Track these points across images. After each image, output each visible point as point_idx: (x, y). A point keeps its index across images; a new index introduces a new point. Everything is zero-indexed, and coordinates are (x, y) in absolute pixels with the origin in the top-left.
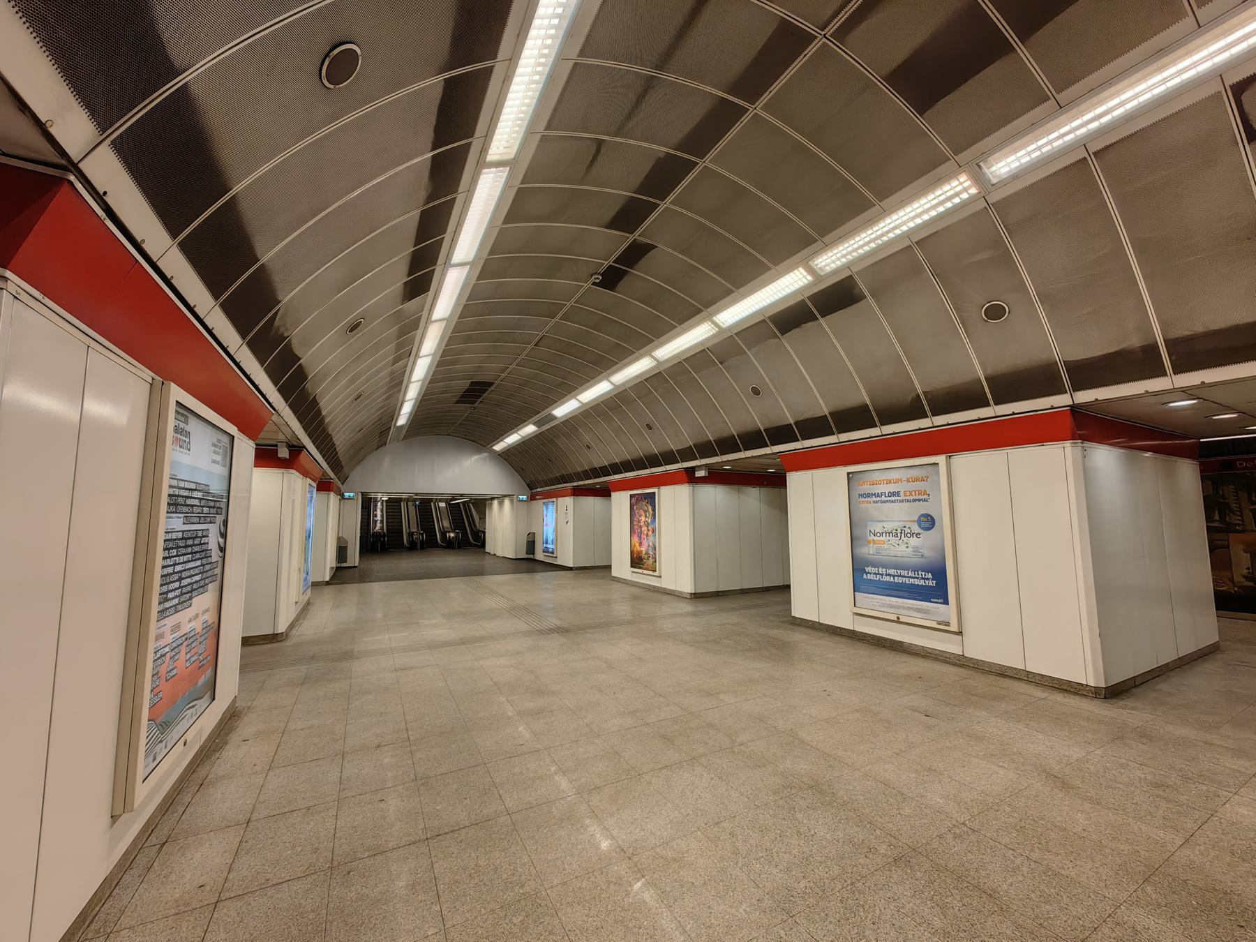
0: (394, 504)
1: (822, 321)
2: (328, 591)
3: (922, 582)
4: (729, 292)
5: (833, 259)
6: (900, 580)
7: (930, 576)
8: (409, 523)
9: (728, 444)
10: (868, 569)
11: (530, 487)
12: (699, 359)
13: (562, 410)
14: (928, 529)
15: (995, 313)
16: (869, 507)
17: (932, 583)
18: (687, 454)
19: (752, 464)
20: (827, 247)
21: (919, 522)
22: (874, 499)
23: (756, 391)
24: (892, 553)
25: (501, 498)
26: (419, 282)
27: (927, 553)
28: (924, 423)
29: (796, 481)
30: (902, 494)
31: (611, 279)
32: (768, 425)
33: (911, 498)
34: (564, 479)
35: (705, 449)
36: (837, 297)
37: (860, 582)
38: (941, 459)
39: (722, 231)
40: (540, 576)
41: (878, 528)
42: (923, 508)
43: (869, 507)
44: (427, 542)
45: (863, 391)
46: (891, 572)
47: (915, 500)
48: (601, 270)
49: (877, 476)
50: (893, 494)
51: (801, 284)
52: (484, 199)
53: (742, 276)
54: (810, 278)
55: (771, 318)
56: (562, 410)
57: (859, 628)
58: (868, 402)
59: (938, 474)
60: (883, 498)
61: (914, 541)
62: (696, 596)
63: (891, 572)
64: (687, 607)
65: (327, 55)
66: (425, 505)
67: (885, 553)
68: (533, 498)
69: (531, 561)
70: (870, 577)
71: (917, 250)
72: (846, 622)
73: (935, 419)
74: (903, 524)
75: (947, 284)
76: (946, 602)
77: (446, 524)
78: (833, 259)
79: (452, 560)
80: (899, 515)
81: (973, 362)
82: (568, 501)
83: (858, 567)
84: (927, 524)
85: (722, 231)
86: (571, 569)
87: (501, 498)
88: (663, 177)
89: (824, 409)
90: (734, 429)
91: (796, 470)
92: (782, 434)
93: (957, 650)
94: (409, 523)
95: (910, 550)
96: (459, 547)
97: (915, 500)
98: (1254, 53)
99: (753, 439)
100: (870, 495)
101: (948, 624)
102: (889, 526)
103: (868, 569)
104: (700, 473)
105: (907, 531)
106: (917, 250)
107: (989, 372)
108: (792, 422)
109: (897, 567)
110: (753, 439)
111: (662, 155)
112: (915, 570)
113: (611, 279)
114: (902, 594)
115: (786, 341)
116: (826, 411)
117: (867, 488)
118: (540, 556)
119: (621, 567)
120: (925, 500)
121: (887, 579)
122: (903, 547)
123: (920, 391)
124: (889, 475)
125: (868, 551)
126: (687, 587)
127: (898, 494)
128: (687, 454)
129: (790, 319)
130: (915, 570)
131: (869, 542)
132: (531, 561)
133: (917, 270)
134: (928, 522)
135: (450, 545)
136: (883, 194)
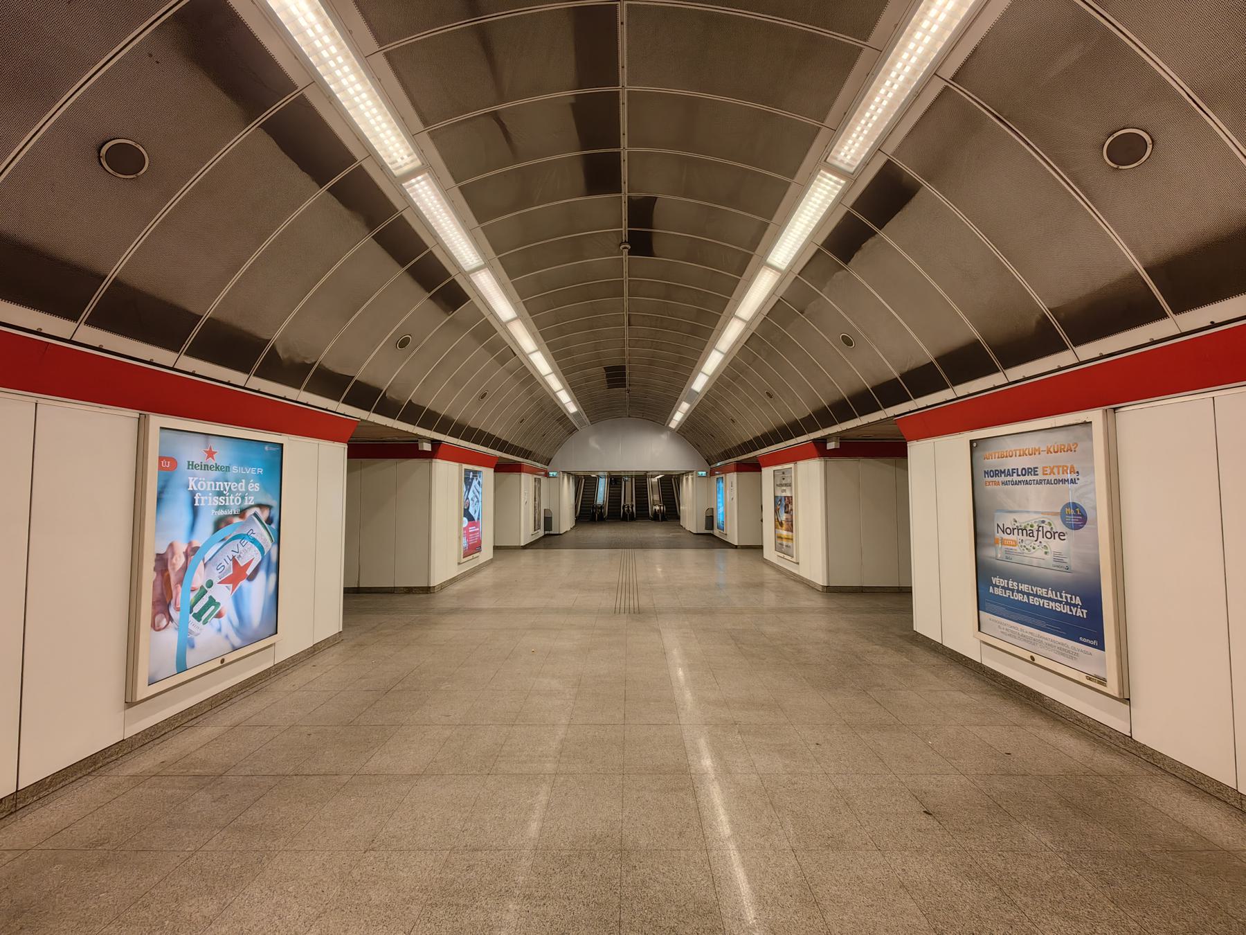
0: (615, 481)
1: (881, 233)
2: (527, 558)
3: (1066, 610)
4: (764, 227)
5: (855, 145)
6: (1036, 601)
7: (1078, 601)
8: (628, 499)
9: (842, 410)
10: (995, 580)
11: (709, 461)
12: (780, 312)
13: (699, 383)
14: (1077, 527)
15: (1127, 150)
16: (993, 488)
17: (1081, 613)
18: (808, 424)
19: (866, 435)
20: (837, 131)
21: (1063, 515)
22: (1003, 478)
23: (847, 342)
24: (1026, 560)
25: (687, 473)
26: (449, 293)
27: (1073, 562)
28: (1065, 359)
29: (918, 450)
30: (1040, 471)
31: (641, 244)
32: (875, 382)
33: (1052, 477)
34: (727, 455)
35: (824, 417)
36: (883, 196)
37: (984, 601)
38: (1095, 416)
39: (710, 158)
40: (718, 553)
41: (1008, 521)
42: (1070, 494)
43: (993, 488)
44: (641, 514)
45: (967, 321)
46: (1024, 587)
47: (1058, 481)
48: (625, 237)
49: (1010, 445)
50: (1026, 471)
51: (837, 192)
52: (434, 208)
53: (770, 207)
54: (843, 182)
55: (826, 244)
56: (699, 383)
57: (988, 663)
58: (978, 337)
59: (1090, 438)
60: (1015, 478)
61: (1055, 545)
62: (830, 590)
63: (1024, 587)
64: (819, 602)
65: (99, 157)
66: (641, 480)
67: (1016, 558)
68: (711, 473)
69: (710, 538)
70: (998, 592)
71: (957, 88)
72: (972, 650)
73: (1079, 350)
74: (1039, 517)
75: (1027, 127)
76: (1101, 647)
77: (656, 497)
78: (855, 145)
79: (657, 532)
80: (1033, 504)
81: (1120, 247)
82: (732, 477)
83: (984, 573)
84: (1072, 520)
85: (710, 158)
86: (736, 547)
87: (687, 473)
88: (595, 123)
89: (927, 355)
90: (842, 391)
91: (917, 439)
92: (890, 392)
93: (1121, 726)
94: (628, 499)
95: (1049, 557)
96: (664, 519)
97: (1058, 481)
98: (305, 7)
99: (863, 402)
100: (998, 473)
101: (1103, 681)
102: (1023, 520)
103: (995, 580)
104: (831, 446)
105: (1047, 528)
106: (957, 88)
107: (1150, 257)
108: (897, 375)
109: (1033, 582)
110: (863, 402)
111: (572, 100)
112: (1057, 588)
113: (641, 244)
114: (1039, 623)
115: (857, 271)
116: (930, 357)
117: (993, 463)
118: (716, 532)
119: (770, 553)
120: (1073, 481)
121: (1019, 597)
122: (1039, 553)
123: (1044, 307)
124: (1021, 441)
125: (994, 554)
126: (820, 579)
127: (1033, 471)
128: (808, 424)
129: (844, 240)
130: (1057, 588)
131: (996, 542)
132: (710, 538)
133: (970, 122)
134: (1077, 517)
135: (656, 517)
136: (864, 31)
